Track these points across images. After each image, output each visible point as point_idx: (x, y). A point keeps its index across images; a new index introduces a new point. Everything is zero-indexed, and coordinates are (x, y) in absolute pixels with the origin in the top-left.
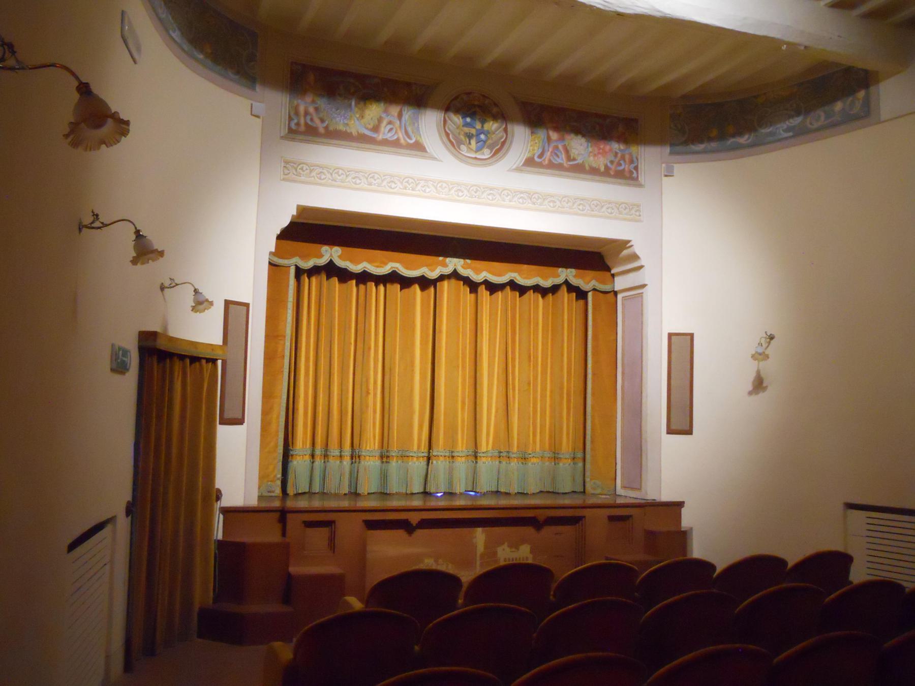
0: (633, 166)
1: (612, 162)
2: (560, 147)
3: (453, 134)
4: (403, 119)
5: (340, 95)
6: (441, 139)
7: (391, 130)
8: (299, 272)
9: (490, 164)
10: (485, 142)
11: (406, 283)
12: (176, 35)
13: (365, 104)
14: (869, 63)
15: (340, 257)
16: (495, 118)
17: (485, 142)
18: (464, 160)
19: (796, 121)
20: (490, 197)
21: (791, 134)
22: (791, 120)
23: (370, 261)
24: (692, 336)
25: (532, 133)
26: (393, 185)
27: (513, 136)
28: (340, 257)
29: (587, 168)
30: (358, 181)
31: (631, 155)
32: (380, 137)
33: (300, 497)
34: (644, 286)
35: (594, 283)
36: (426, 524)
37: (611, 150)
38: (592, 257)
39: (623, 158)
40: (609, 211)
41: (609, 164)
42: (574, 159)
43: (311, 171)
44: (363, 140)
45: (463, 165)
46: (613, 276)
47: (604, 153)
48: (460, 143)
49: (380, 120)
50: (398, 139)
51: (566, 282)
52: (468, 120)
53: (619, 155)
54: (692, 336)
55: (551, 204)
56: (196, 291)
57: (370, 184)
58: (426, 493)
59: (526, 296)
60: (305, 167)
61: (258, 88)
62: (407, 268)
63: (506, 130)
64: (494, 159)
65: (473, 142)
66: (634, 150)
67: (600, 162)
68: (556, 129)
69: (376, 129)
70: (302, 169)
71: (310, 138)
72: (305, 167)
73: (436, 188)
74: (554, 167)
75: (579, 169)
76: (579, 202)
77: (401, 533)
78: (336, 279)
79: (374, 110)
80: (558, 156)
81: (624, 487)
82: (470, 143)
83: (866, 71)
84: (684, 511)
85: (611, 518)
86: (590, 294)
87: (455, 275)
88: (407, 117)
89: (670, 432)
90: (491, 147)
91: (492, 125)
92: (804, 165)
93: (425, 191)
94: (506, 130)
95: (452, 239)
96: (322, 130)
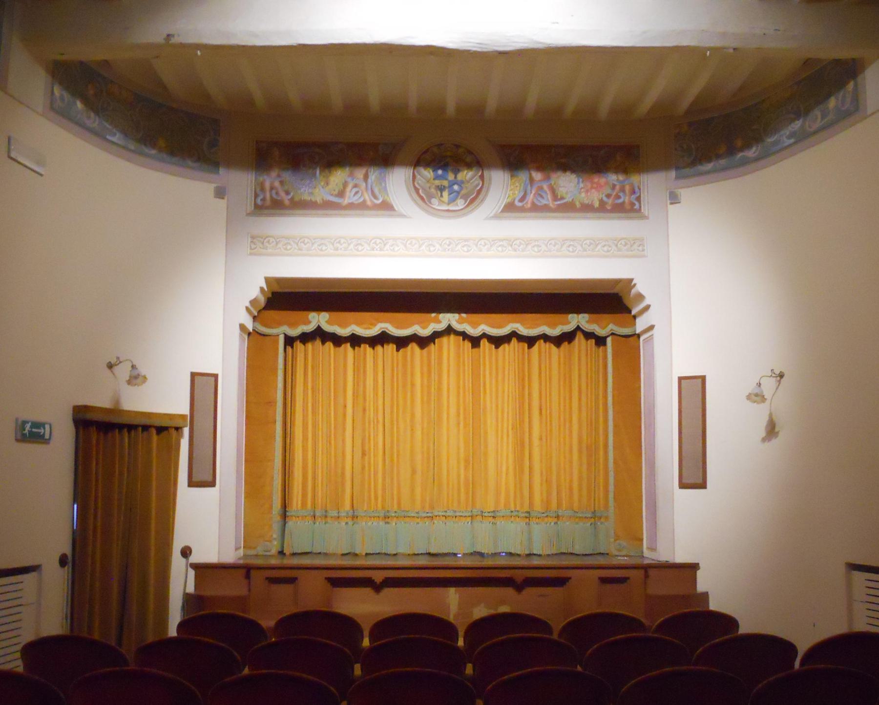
0: (634, 197)
1: (608, 196)
2: (545, 187)
3: (423, 189)
4: (369, 181)
5: (304, 166)
6: (411, 195)
7: (356, 193)
8: (289, 341)
9: (464, 215)
10: (458, 193)
11: (401, 343)
12: (117, 138)
13: (330, 172)
14: (844, 53)
15: (328, 322)
16: (469, 166)
17: (458, 193)
18: (436, 213)
19: (797, 125)
20: (465, 249)
21: (792, 141)
22: (792, 125)
23: (358, 324)
24: (703, 379)
25: (512, 176)
26: (360, 248)
27: (490, 183)
28: (328, 322)
29: (578, 205)
30: (324, 248)
31: (632, 186)
32: (346, 201)
33: (369, 557)
34: (652, 328)
35: (611, 327)
36: (391, 583)
37: (607, 183)
38: (609, 301)
39: (623, 190)
40: (605, 249)
41: (605, 199)
42: (562, 198)
43: (277, 243)
44: (328, 207)
45: (435, 219)
46: (635, 317)
47: (599, 187)
48: (431, 197)
49: (345, 185)
50: (364, 201)
51: (578, 328)
52: (440, 172)
53: (618, 187)
54: (703, 379)
55: (536, 249)
56: (133, 367)
57: (337, 249)
58: (281, 553)
59: (536, 348)
60: (271, 240)
61: (222, 171)
62: (397, 327)
63: (482, 177)
64: (469, 209)
65: (445, 194)
66: (635, 179)
67: (595, 197)
68: (539, 169)
69: (341, 194)
70: (268, 242)
71: (278, 211)
72: (271, 240)
73: (405, 246)
74: (537, 209)
75: (568, 208)
76: (568, 243)
77: (367, 591)
78: (331, 344)
79: (339, 176)
80: (542, 197)
81: (648, 548)
82: (442, 196)
83: (853, 60)
84: (699, 574)
85: (604, 580)
86: (609, 340)
87: (449, 330)
88: (373, 177)
89: (683, 486)
90: (465, 197)
91: (466, 175)
92: (803, 174)
93: (393, 250)
94: (482, 177)
95: (445, 294)
96: (287, 202)
